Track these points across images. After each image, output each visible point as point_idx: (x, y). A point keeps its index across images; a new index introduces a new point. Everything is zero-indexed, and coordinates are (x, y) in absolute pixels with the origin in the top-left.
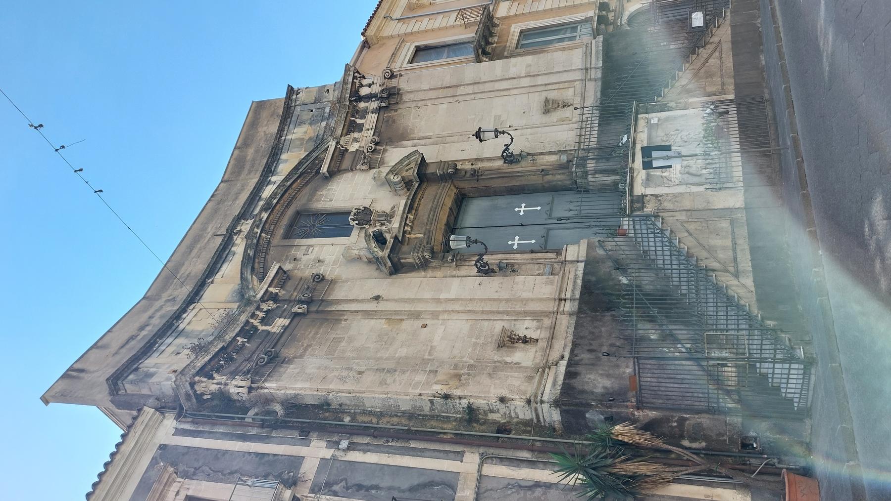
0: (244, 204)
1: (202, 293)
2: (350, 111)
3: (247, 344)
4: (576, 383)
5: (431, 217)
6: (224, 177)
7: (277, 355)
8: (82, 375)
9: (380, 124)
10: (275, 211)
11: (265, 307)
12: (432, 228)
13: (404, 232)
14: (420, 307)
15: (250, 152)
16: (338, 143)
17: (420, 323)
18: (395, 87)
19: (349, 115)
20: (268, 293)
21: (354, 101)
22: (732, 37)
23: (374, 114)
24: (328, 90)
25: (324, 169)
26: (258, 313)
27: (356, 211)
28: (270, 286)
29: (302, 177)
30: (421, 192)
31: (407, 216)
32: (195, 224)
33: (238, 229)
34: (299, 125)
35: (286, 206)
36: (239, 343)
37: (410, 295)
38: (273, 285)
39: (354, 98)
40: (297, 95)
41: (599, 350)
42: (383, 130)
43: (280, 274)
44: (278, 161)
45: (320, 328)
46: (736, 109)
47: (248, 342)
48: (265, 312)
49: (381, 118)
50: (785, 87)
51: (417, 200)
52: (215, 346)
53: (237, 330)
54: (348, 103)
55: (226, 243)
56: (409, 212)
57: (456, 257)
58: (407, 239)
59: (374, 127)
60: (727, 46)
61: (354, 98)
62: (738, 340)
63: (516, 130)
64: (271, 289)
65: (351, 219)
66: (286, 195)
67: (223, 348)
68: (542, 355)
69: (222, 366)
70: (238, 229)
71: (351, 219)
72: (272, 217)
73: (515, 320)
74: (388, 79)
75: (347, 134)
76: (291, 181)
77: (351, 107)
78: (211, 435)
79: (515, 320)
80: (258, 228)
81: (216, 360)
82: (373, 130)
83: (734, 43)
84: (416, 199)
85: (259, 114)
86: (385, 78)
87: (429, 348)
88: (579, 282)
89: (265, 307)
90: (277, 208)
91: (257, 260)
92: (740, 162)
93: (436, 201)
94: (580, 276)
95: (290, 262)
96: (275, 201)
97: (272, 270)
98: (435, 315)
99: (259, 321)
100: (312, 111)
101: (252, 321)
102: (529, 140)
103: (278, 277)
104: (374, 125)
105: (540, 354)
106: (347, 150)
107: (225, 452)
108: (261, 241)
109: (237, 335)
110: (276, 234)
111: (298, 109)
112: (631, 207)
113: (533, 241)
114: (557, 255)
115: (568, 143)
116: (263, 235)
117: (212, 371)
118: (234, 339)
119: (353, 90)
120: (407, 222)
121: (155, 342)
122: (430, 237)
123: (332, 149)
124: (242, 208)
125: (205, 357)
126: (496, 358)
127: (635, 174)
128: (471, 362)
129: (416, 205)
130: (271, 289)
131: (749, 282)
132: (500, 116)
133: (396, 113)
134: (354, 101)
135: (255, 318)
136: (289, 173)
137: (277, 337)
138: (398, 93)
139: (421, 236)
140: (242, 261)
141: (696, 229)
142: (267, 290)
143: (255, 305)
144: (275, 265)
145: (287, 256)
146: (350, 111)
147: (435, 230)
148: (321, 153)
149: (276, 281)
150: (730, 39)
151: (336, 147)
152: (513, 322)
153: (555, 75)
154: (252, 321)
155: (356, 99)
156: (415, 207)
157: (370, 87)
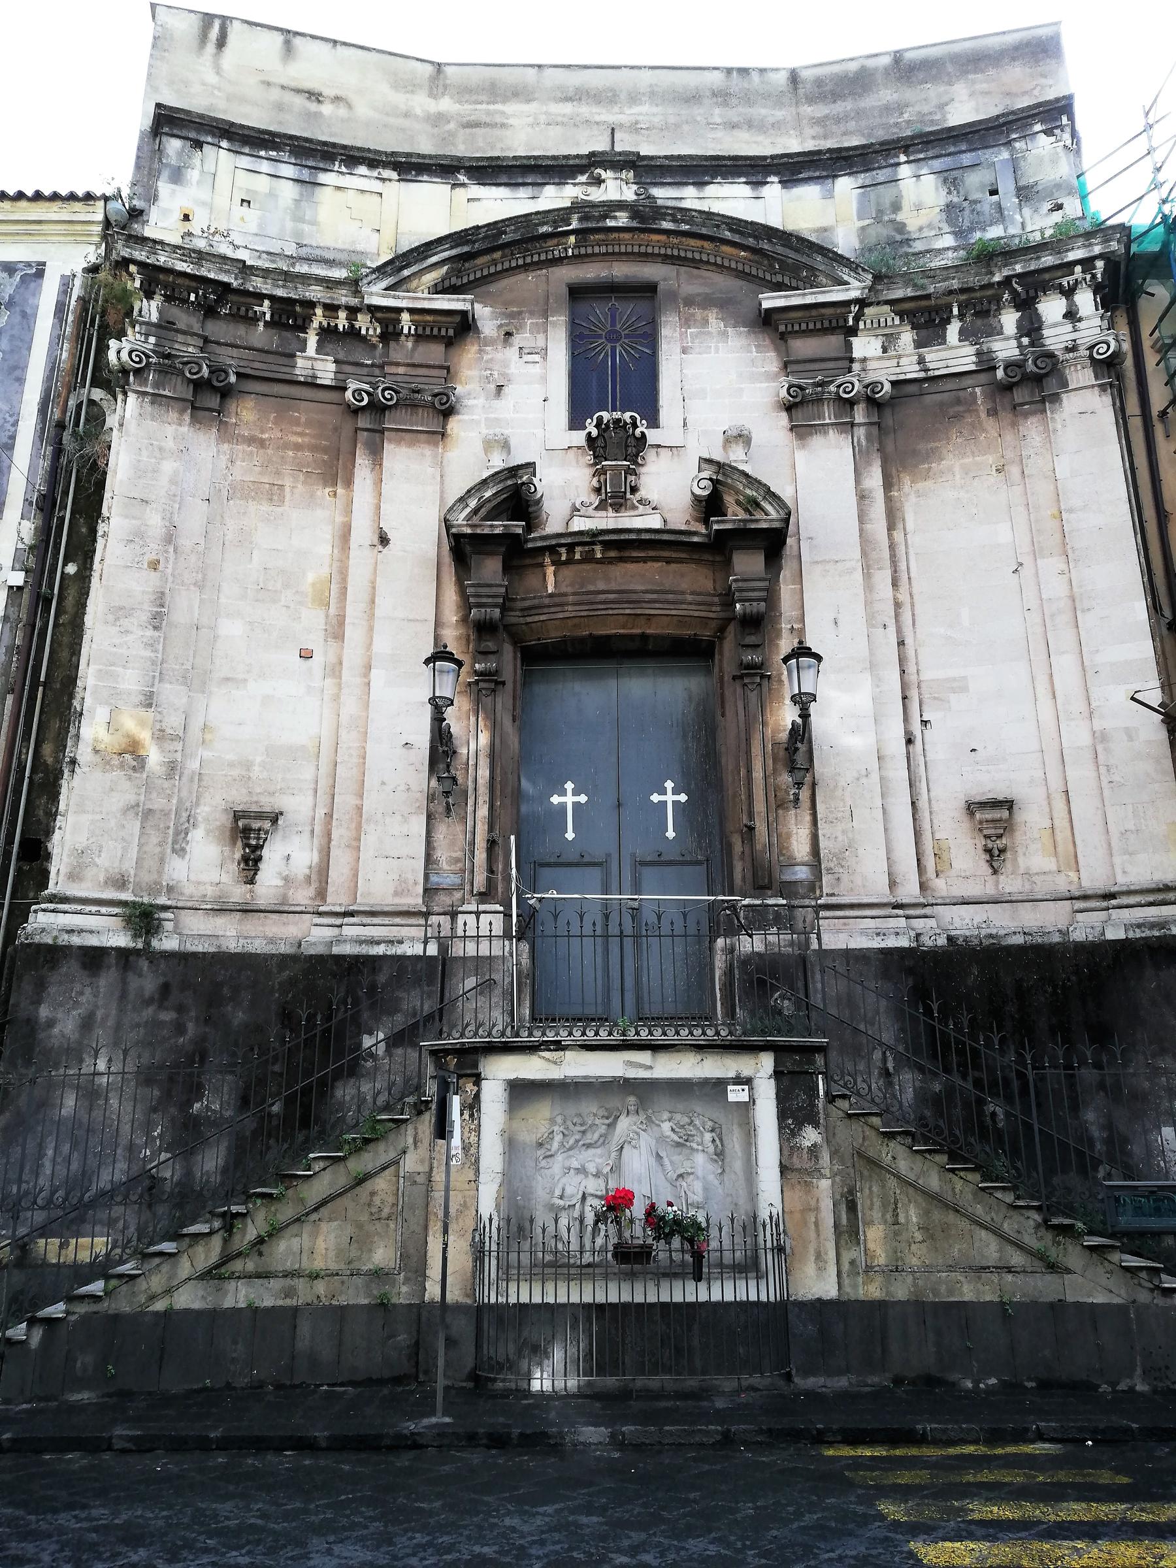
0: (679, 157)
1: (425, 178)
2: (978, 294)
3: (261, 324)
4: (71, 967)
5: (602, 597)
6: (907, 50)
7: (226, 393)
8: (211, 47)
9: (950, 385)
10: (645, 236)
11: (363, 322)
12: (570, 608)
13: (552, 550)
14: (354, 633)
15: (886, 95)
16: (862, 303)
17: (315, 642)
18: (1064, 384)
19: (963, 297)
20: (393, 315)
21: (1014, 292)
22: (1078, 1305)
23: (974, 359)
24: (1059, 207)
25: (771, 301)
26: (342, 315)
27: (629, 421)
28: (412, 311)
29: (756, 258)
30: (683, 555)
31: (593, 543)
32: (651, 72)
33: (604, 175)
34: (945, 181)
35: (666, 255)
36: (257, 308)
37: (384, 605)
38: (416, 317)
39: (1019, 289)
40: (1045, 132)
41: (166, 1004)
42: (928, 399)
43: (449, 319)
44: (827, 177)
45: (313, 448)
46: (772, 1299)
47: (266, 324)
48: (352, 326)
49: (968, 381)
50: (1131, 1429)
51: (651, 553)
52: (221, 269)
53: (280, 293)
54: (997, 278)
55: (562, 166)
56: (607, 545)
57: (485, 681)
58: (540, 560)
59: (931, 373)
60: (1045, 1287)
61: (1019, 289)
62: (536, 1265)
63: (909, 741)
64: (405, 317)
65: (600, 419)
66: (693, 242)
67: (227, 286)
68: (205, 896)
69: (186, 301)
70: (604, 175)
71: (600, 419)
72: (627, 236)
73: (312, 831)
74: (1091, 357)
75: (901, 314)
76: (737, 238)
77: (990, 292)
78: (57, 340)
79: (312, 831)
80: (580, 220)
81: (194, 284)
82: (922, 375)
83: (1058, 1308)
84: (653, 549)
85: (1014, 59)
86: (1091, 348)
87: (241, 676)
88: (380, 950)
89: (363, 322)
90: (655, 237)
91: (497, 255)
92: (707, 1299)
93: (654, 596)
94: (399, 950)
95: (500, 326)
96: (666, 225)
97: (449, 300)
98: (335, 670)
99: (325, 324)
100: (994, 192)
101: (319, 311)
102: (864, 780)
103: (439, 318)
104: (937, 373)
105: (209, 893)
106: (853, 331)
107: (21, 381)
108: (551, 242)
109: (272, 298)
110: (585, 266)
111: (1005, 155)
112: (446, 1052)
113: (570, 835)
114: (480, 894)
115: (845, 878)
116: (572, 239)
117: (165, 288)
118: (260, 297)
119: (1047, 276)
120: (578, 549)
121: (276, 147)
122: (546, 610)
123: (837, 295)
124: (666, 157)
125: (185, 261)
126: (203, 811)
127: (546, 1054)
128: (193, 765)
129: (635, 554)
130: (405, 317)
131: (188, 1299)
132: (964, 689)
133: (983, 415)
134: (1014, 292)
135: (327, 313)
136: (752, 223)
137: (288, 377)
138: (1043, 401)
139: (550, 589)
140: (477, 228)
141: (373, 1194)
142: (399, 310)
143: (354, 301)
144: (464, 300)
145: (520, 313)
146: (978, 294)
147: (567, 615)
148: (827, 276)
149: (429, 318)
150: (1070, 1299)
151: (846, 304)
152: (308, 828)
153: (1066, 808)
154: (319, 311)
155: (1018, 294)
156: (627, 554)
157: (1065, 316)
